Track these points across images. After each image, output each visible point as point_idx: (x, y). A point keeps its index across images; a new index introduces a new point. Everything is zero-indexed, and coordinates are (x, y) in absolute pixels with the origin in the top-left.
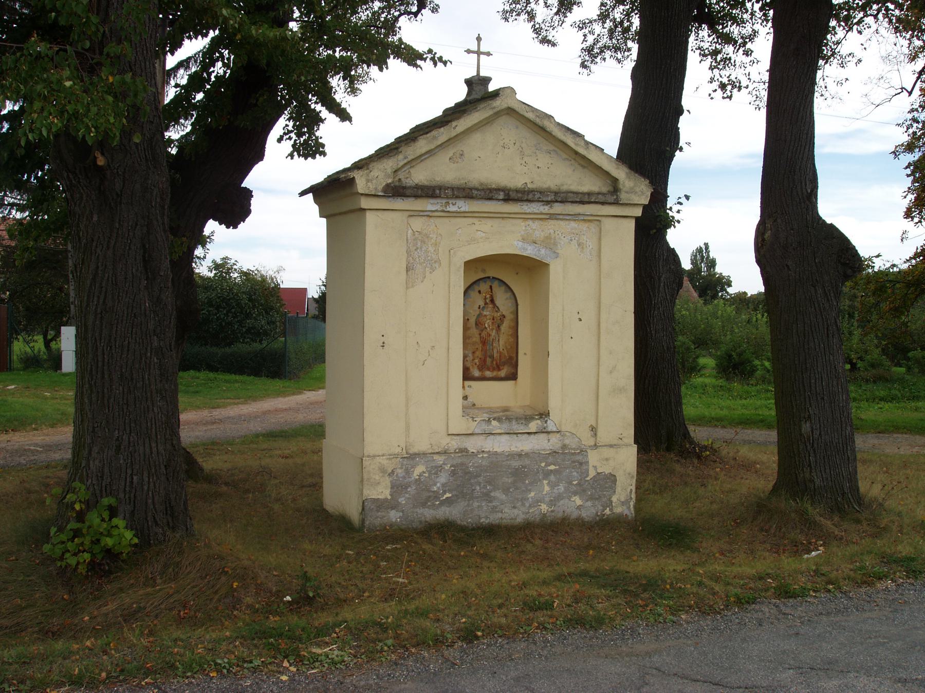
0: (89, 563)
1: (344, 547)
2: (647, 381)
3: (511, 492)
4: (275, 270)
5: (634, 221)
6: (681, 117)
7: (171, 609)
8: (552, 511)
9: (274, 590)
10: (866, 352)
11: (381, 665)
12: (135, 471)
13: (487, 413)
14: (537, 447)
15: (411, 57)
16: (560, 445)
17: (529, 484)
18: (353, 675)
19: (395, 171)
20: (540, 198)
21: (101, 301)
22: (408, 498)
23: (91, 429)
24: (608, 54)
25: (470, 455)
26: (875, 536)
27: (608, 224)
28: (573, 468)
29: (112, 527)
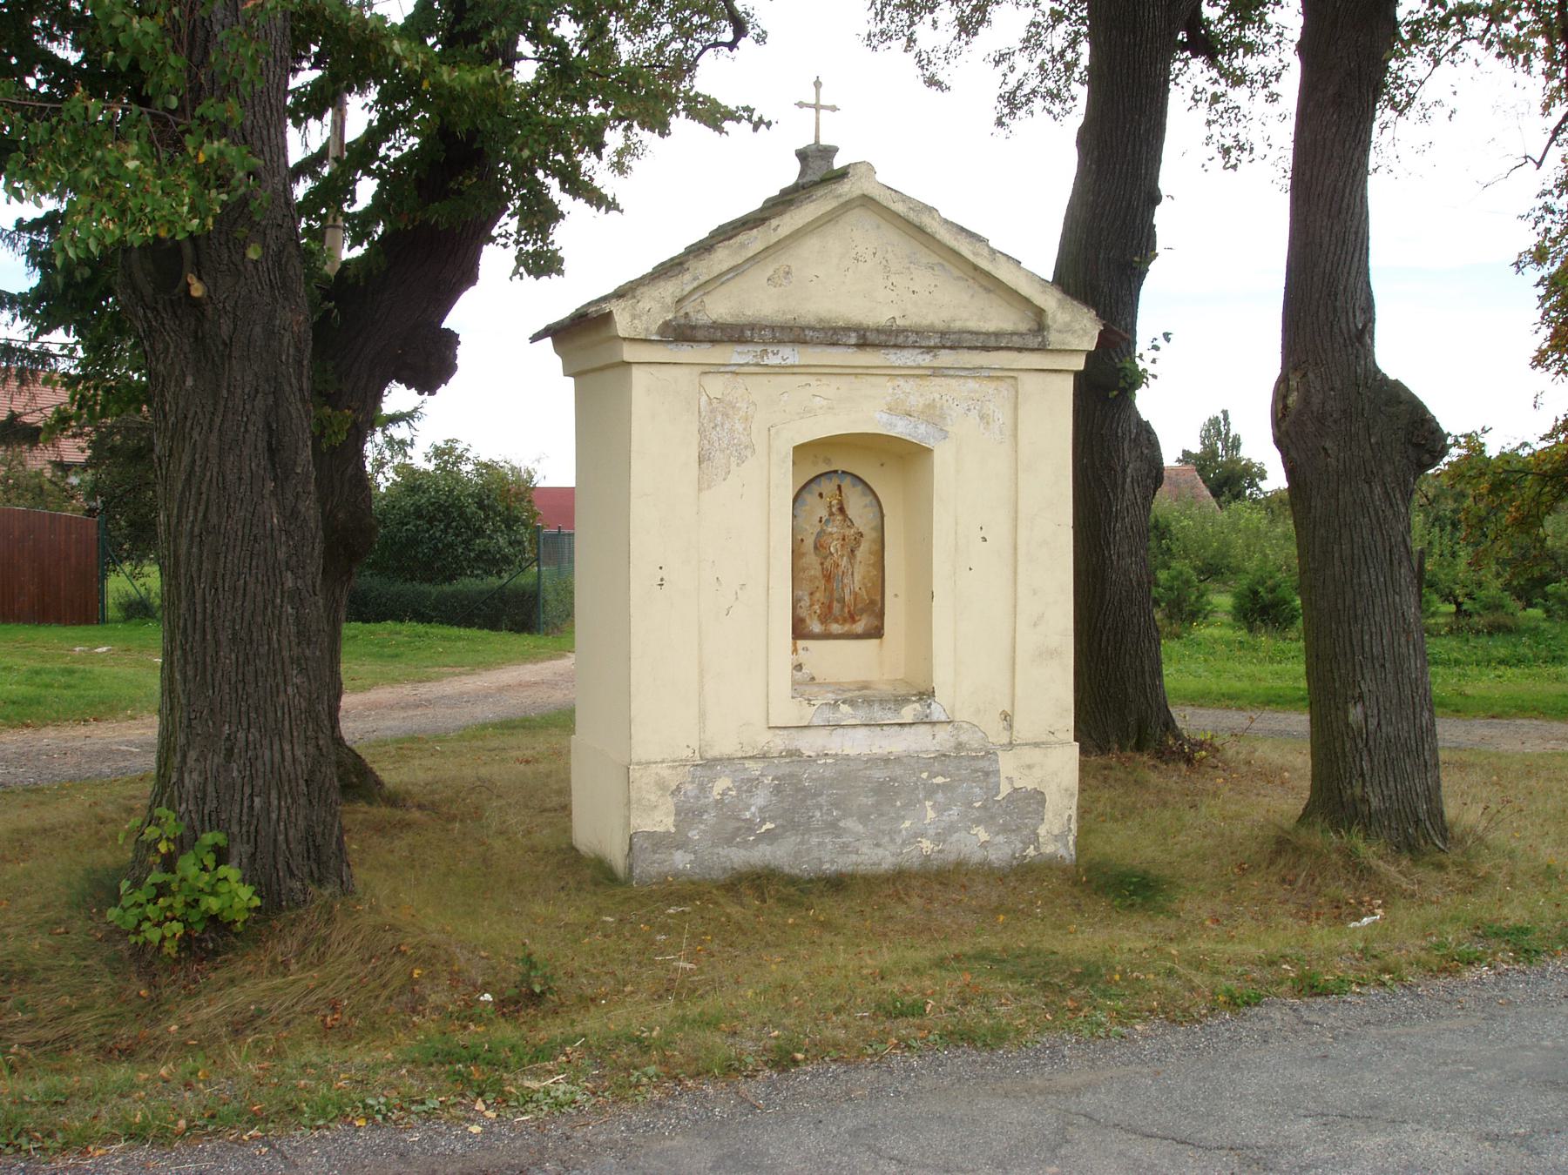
0: (181, 939)
1: (599, 911)
2: (1104, 638)
5: (1072, 378)
6: (1158, 209)
7: (312, 1013)
8: (940, 851)
9: (480, 982)
10: (1480, 585)
11: (635, 1108)
12: (257, 790)
14: (914, 747)
15: (713, 115)
18: (589, 1124)
21: (200, 515)
23: (185, 721)
24: (1038, 104)
26: (1466, 891)
27: (1029, 383)
29: (219, 880)
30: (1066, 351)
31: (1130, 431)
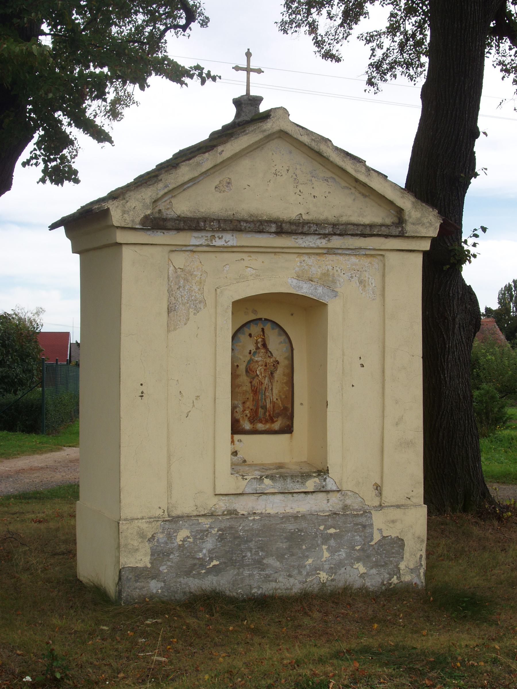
1: (98, 623)
2: (441, 434)
3: (286, 559)
4: (35, 312)
6: (477, 141)
8: (333, 580)
13: (259, 470)
14: (315, 508)
16: (341, 506)
17: (306, 549)
19: (155, 201)
20: (316, 230)
22: (171, 566)
24: (398, 70)
25: (241, 518)
27: (392, 258)
28: (356, 532)
30: (417, 237)
31: (458, 292)
